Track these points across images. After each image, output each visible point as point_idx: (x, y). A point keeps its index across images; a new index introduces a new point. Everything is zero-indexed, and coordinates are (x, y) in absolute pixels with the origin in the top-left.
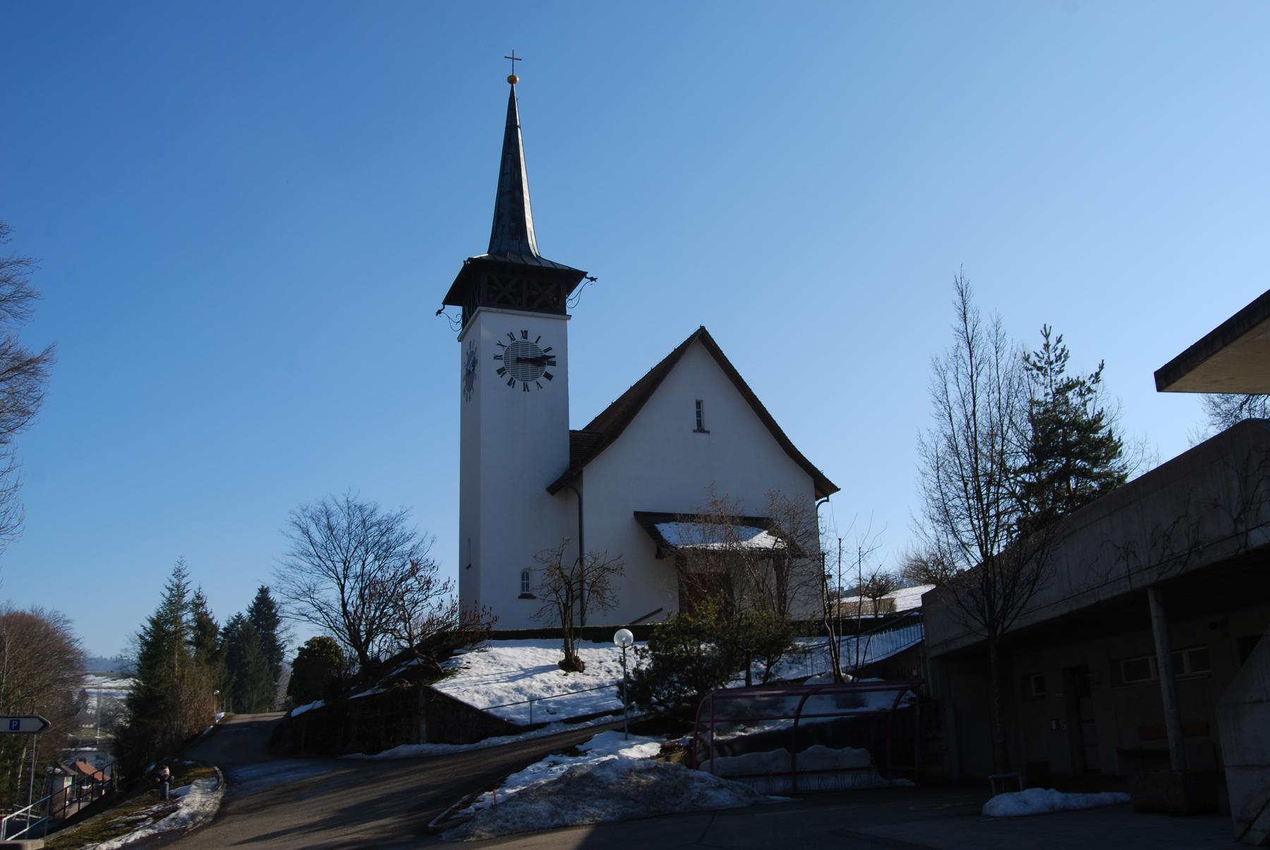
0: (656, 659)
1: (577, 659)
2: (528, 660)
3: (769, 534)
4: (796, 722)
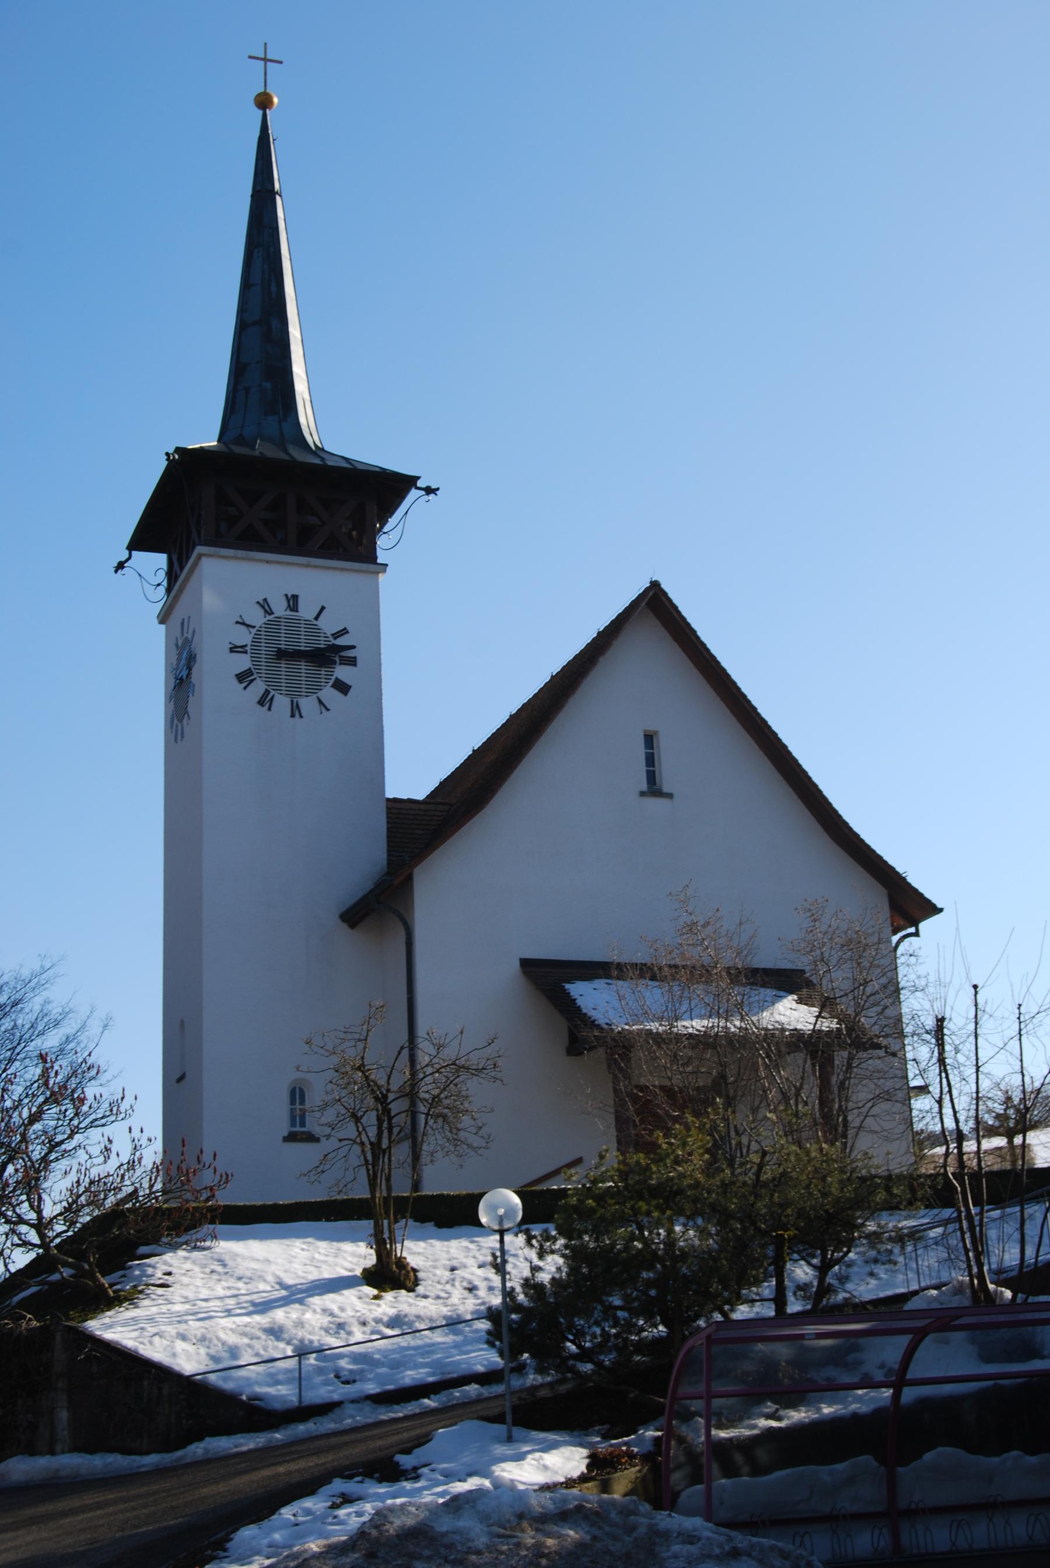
0: (575, 1256)
1: (401, 1263)
2: (297, 1267)
3: (800, 1001)
4: (897, 1396)
